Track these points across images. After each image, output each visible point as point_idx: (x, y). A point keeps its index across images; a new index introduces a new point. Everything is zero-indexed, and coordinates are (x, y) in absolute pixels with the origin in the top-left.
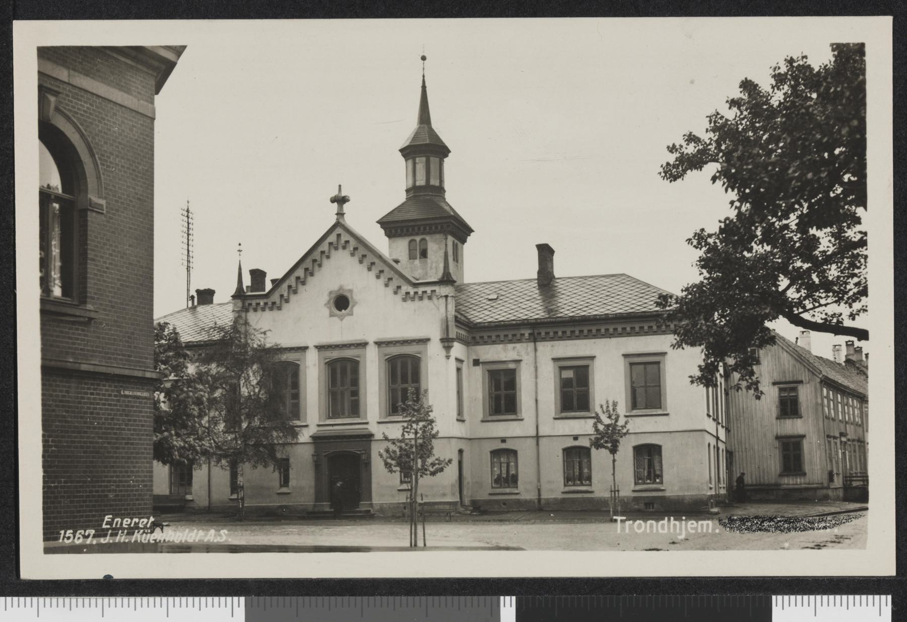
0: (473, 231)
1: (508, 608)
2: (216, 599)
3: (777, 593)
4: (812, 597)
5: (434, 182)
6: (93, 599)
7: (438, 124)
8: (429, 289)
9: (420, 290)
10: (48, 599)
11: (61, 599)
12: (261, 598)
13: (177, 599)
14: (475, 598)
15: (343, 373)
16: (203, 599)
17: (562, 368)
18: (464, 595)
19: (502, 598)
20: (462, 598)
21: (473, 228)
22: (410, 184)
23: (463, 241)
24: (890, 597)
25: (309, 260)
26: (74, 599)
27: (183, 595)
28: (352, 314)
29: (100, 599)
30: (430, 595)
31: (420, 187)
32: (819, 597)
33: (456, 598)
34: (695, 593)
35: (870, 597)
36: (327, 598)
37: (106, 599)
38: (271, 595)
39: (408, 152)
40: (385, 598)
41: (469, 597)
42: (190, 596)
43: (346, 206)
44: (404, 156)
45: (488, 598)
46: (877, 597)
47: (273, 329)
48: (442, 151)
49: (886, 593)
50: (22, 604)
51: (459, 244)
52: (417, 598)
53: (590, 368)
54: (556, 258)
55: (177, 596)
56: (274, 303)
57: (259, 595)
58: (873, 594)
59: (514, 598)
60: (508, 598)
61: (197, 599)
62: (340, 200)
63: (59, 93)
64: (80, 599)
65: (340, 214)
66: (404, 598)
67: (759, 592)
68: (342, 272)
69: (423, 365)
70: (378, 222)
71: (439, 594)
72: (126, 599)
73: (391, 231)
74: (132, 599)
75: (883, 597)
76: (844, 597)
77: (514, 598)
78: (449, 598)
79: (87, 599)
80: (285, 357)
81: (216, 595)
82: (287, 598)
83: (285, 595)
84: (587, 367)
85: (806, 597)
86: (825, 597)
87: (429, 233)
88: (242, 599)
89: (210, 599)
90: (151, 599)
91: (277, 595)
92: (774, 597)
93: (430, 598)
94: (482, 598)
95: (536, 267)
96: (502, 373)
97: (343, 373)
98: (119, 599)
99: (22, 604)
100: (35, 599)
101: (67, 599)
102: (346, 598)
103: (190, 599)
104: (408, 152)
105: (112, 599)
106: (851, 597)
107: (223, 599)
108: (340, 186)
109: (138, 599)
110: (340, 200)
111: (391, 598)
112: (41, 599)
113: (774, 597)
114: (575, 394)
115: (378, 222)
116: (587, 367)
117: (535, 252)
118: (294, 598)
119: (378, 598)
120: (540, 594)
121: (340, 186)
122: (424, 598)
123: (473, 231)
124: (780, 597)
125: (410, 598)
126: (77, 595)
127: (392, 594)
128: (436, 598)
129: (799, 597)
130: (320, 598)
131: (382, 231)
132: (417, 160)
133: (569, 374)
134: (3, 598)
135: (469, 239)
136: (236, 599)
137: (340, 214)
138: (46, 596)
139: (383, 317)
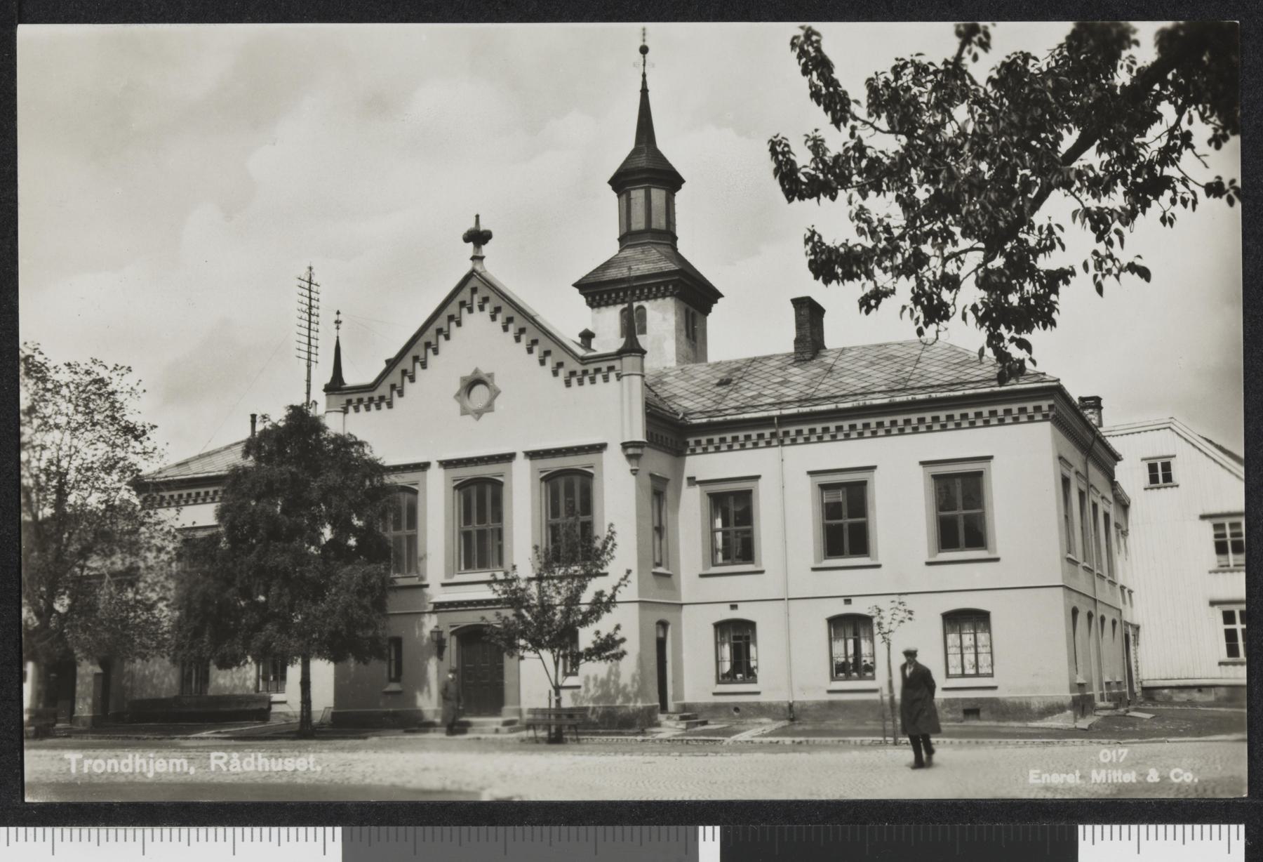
0: (721, 296)
1: (709, 843)
2: (302, 829)
3: (1085, 822)
4: (1134, 827)
5: (659, 222)
6: (130, 830)
7: (664, 143)
8: (604, 366)
9: (591, 368)
10: (67, 830)
11: (85, 830)
12: (365, 829)
13: (247, 830)
14: (664, 828)
15: (480, 496)
16: (284, 830)
17: (824, 487)
18: (649, 824)
19: (701, 828)
20: (646, 828)
21: (721, 290)
22: (625, 230)
23: (707, 311)
24: (1242, 827)
25: (431, 332)
26: (103, 830)
27: (255, 825)
28: (1138, 628)
29: (139, 830)
30: (601, 824)
31: (639, 233)
32: (1143, 827)
33: (637, 828)
34: (971, 821)
35: (1215, 827)
36: (457, 828)
37: (148, 830)
38: (379, 824)
39: (621, 182)
40: (537, 829)
41: (655, 827)
42: (265, 825)
43: (486, 249)
44: (614, 189)
45: (682, 828)
46: (1224, 827)
47: (383, 437)
48: (671, 181)
49: (1237, 822)
50: (31, 837)
51: (698, 315)
52: (582, 828)
53: (869, 486)
54: (827, 320)
55: (247, 825)
56: (382, 398)
57: (361, 824)
58: (1219, 823)
59: (717, 828)
60: (709, 829)
61: (275, 830)
62: (478, 237)
63: (719, 385)
64: (112, 830)
65: (477, 258)
66: (564, 828)
67: (1056, 823)
68: (478, 341)
69: (596, 484)
70: (575, 285)
71: (613, 824)
72: (175, 830)
73: (594, 299)
74: (184, 830)
75: (1234, 827)
76: (1179, 827)
77: (717, 828)
78: (627, 828)
79: (121, 830)
80: (390, 479)
81: (301, 825)
82: (401, 829)
83: (397, 824)
84: (864, 483)
85: (1125, 827)
86: (1152, 827)
87: (647, 299)
88: (338, 830)
89: (293, 829)
90: (211, 830)
91: (387, 824)
92: (1080, 827)
93: (600, 828)
94: (673, 828)
95: (792, 333)
96: (731, 499)
97: (480, 496)
98: (166, 830)
99: (31, 837)
100: (49, 830)
101: (94, 830)
102: (483, 829)
103: (266, 830)
104: (621, 182)
105: (157, 830)
106: (1188, 827)
107: (311, 829)
108: (477, 216)
109: (193, 830)
110: (478, 237)
111: (546, 829)
112: (58, 830)
113: (1080, 827)
114: (845, 524)
115: (575, 285)
116: (864, 483)
117: (791, 311)
118: (410, 829)
119: (528, 828)
120: (754, 823)
121: (477, 216)
122: (591, 829)
123: (721, 296)
124: (1089, 827)
125: (573, 829)
126: (107, 825)
127: (547, 823)
128: (609, 828)
129: (1116, 827)
130: (447, 829)
131: (582, 299)
132: (634, 194)
133: (840, 496)
134: (4, 829)
135: (715, 307)
136: (329, 829)
137: (477, 258)
138: (64, 825)
139: (539, 415)
